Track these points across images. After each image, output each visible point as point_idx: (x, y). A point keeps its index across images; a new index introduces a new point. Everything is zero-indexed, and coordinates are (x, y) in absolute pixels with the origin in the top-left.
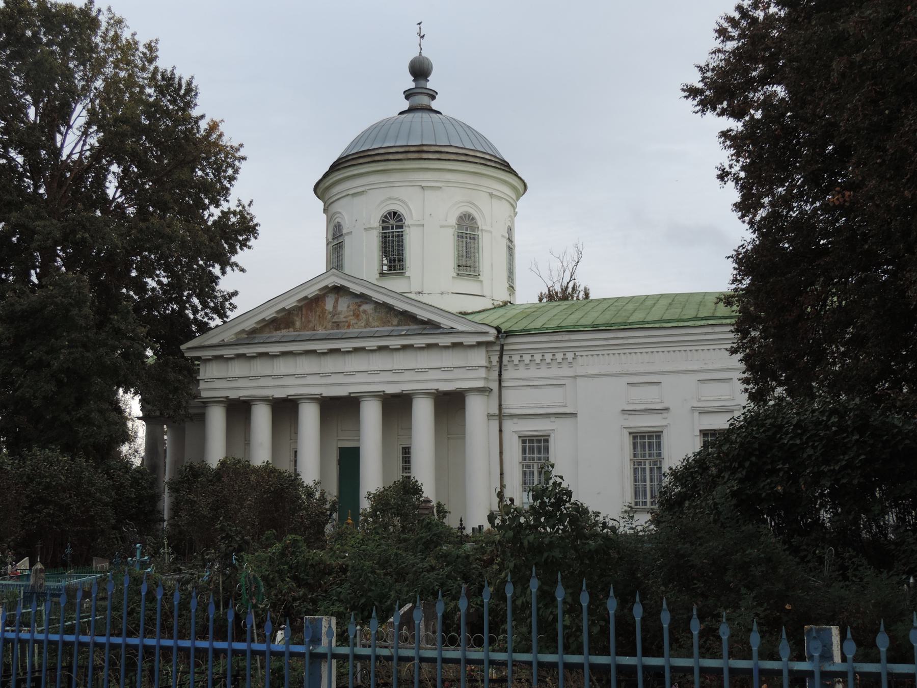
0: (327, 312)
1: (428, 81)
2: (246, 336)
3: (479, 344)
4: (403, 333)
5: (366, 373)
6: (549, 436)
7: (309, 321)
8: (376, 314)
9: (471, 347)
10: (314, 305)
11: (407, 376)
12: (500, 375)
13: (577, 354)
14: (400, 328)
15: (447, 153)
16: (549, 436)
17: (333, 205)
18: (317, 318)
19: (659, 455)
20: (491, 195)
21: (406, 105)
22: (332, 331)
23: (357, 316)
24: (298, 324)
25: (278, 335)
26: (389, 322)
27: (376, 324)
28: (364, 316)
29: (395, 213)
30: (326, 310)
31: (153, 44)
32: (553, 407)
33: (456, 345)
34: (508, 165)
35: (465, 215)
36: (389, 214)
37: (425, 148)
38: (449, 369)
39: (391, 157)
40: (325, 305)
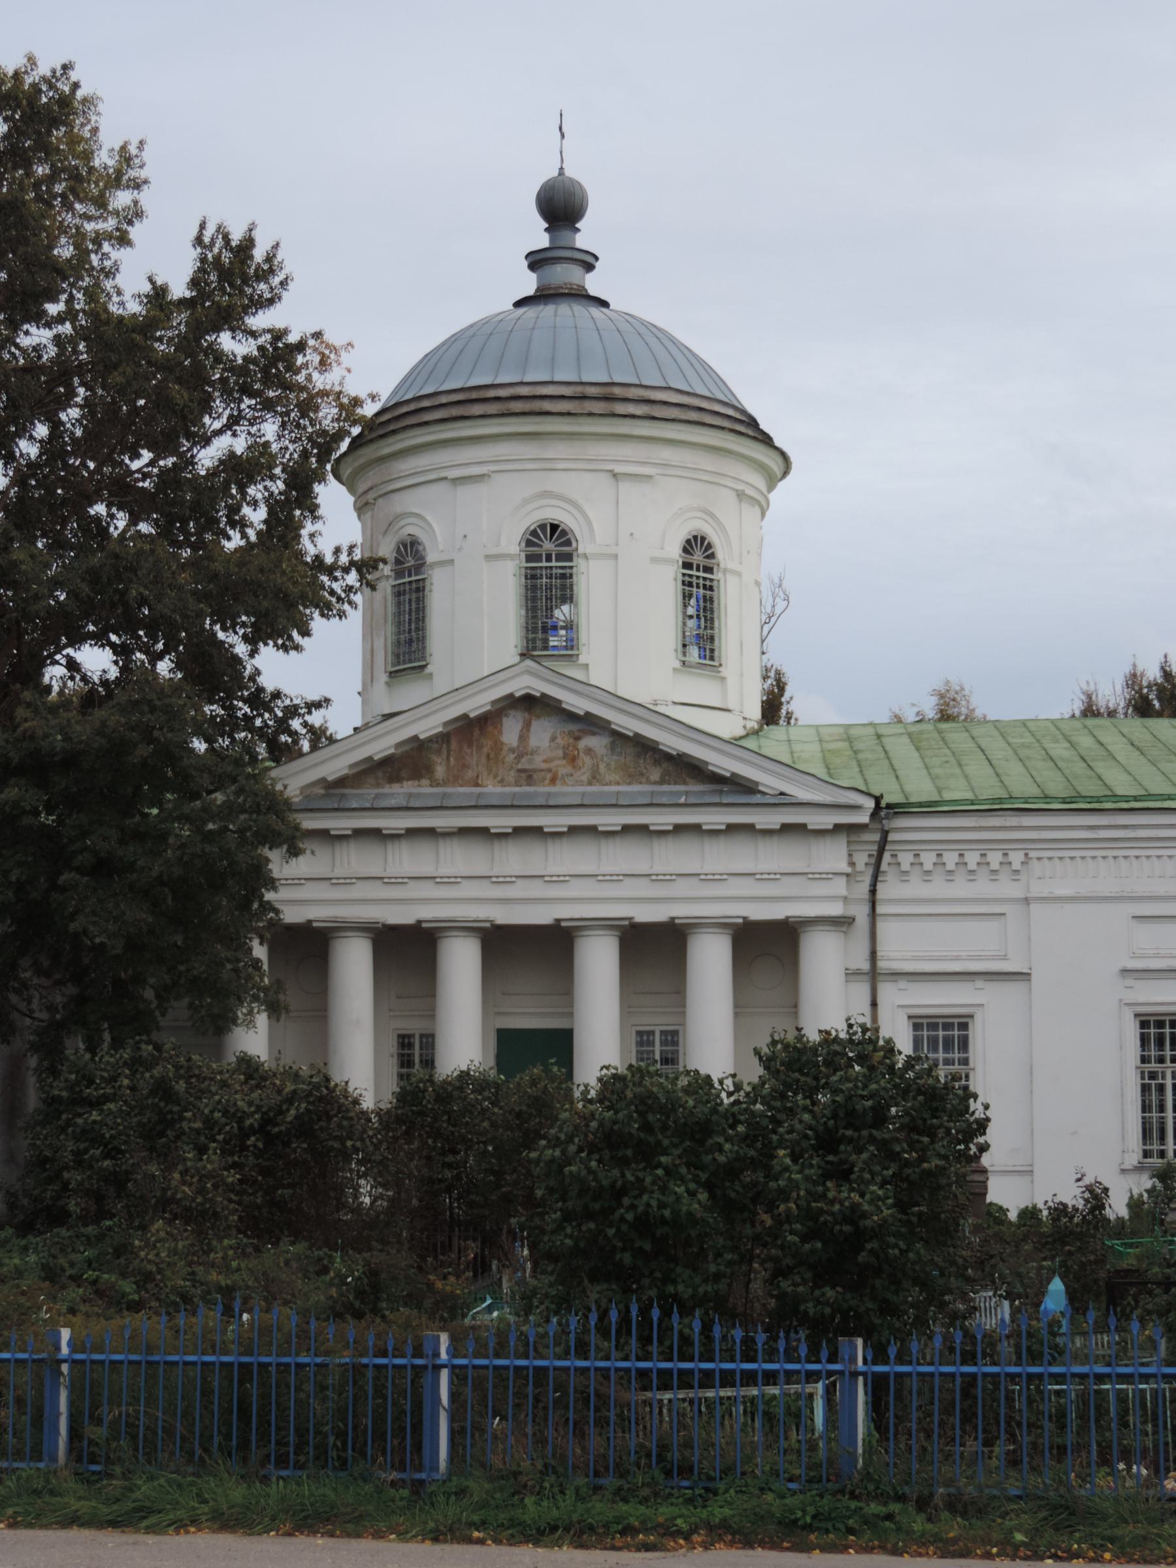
0: (505, 748)
1: (578, 230)
2: (322, 791)
3: (838, 828)
4: (682, 800)
5: (592, 880)
6: (971, 1016)
7: (465, 766)
8: (615, 757)
9: (820, 833)
10: (476, 732)
11: (682, 888)
12: (873, 891)
13: (1032, 854)
14: (665, 788)
15: (665, 403)
16: (971, 1016)
17: (397, 497)
18: (484, 760)
19: (965, 1062)
20: (740, 495)
21: (528, 284)
22: (517, 789)
23: (572, 760)
24: (440, 771)
25: (399, 792)
26: (642, 774)
27: (614, 777)
28: (588, 761)
29: (554, 527)
30: (502, 743)
31: (133, 150)
32: (979, 958)
33: (787, 829)
34: (753, 423)
35: (695, 537)
36: (542, 527)
37: (617, 391)
38: (772, 876)
39: (547, 406)
40: (500, 732)
